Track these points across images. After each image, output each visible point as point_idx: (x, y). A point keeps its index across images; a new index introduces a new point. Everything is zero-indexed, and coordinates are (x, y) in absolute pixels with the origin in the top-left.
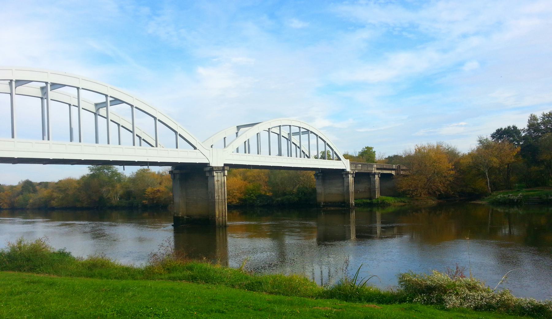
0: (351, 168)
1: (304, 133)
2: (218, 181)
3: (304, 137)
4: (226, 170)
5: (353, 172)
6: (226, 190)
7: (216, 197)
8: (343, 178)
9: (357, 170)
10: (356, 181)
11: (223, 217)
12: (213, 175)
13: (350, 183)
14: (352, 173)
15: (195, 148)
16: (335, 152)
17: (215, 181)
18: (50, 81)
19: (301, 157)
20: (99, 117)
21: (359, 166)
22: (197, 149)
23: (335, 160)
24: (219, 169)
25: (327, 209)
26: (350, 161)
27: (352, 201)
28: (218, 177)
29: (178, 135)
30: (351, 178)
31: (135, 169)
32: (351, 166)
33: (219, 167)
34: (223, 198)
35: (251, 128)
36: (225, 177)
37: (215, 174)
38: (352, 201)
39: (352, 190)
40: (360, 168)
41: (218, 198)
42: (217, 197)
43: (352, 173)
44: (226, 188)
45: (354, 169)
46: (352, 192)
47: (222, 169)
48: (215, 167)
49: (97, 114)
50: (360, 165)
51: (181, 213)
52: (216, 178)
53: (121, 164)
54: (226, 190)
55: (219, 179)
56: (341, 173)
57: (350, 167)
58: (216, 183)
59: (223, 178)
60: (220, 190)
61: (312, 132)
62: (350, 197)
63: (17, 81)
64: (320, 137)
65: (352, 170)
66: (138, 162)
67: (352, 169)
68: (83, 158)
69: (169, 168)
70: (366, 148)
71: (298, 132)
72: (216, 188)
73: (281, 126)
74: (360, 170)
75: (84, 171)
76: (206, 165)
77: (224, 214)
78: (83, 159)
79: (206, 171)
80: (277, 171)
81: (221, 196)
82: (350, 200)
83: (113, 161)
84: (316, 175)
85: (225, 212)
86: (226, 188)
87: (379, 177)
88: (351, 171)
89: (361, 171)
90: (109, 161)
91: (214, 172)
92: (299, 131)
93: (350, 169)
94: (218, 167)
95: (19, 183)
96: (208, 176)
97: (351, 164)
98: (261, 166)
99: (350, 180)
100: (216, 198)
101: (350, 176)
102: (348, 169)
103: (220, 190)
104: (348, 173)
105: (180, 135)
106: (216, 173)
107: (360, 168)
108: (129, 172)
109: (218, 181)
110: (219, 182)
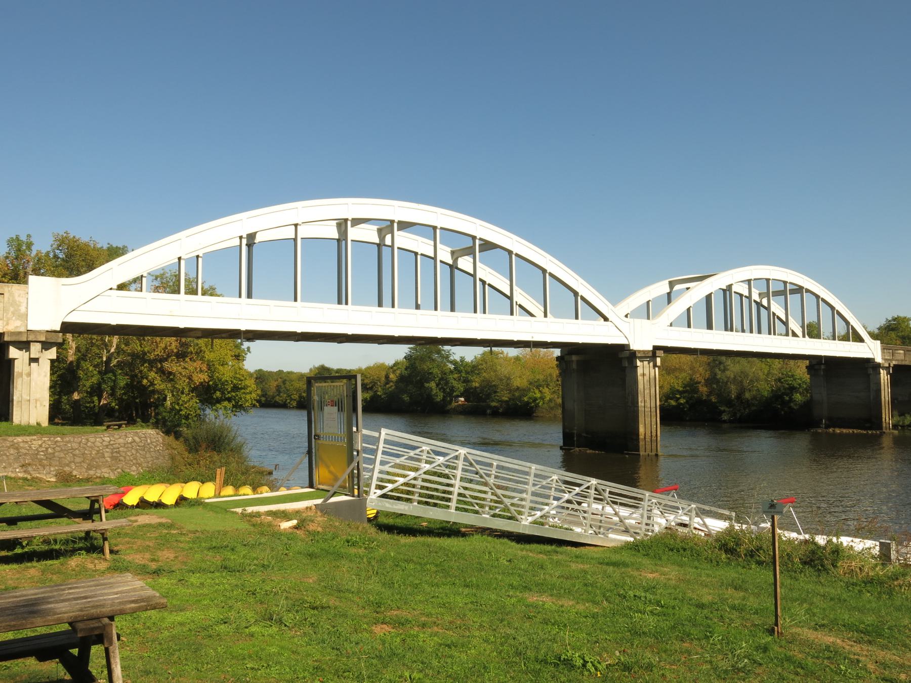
0: (885, 356)
1: (793, 292)
2: (644, 375)
3: (794, 300)
4: (659, 357)
5: (889, 364)
6: (658, 392)
7: (640, 404)
8: (868, 375)
9: (896, 360)
10: (894, 382)
11: (653, 438)
12: (634, 365)
13: (882, 384)
14: (887, 365)
15: (606, 319)
16: (852, 326)
17: (639, 374)
18: (805, 287)
19: (751, 332)
20: (456, 271)
21: (899, 353)
22: (610, 320)
23: (823, 339)
24: (647, 355)
25: (834, 431)
26: (881, 344)
27: (887, 419)
28: (644, 369)
29: (579, 298)
30: (884, 376)
31: (478, 351)
32: (883, 352)
33: (646, 351)
34: (653, 405)
35: (698, 285)
36: (657, 369)
37: (639, 363)
38: (887, 419)
39: (887, 399)
40: (902, 357)
41: (643, 404)
42: (641, 402)
43: (887, 365)
44: (657, 388)
45: (889, 358)
46: (887, 402)
47: (650, 354)
48: (639, 351)
49: (454, 266)
50: (902, 352)
51: (576, 428)
52: (640, 371)
53: (488, 345)
54: (658, 392)
55: (646, 372)
56: (865, 366)
57: (882, 355)
58: (640, 378)
59: (652, 371)
60: (647, 391)
61: (808, 291)
62: (883, 411)
63: (400, 223)
64: (823, 300)
65: (885, 360)
66: (302, 333)
67: (886, 357)
68: (397, 333)
69: (557, 352)
70: (894, 319)
71: (471, 247)
72: (641, 386)
73: (751, 280)
74: (902, 360)
75: (399, 353)
76: (623, 348)
77: (654, 434)
78: (300, 332)
79: (622, 358)
80: (729, 362)
81: (648, 401)
82: (884, 416)
83: (185, 328)
84: (810, 368)
85: (657, 430)
86: (657, 388)
87: (890, 374)
88: (883, 362)
89: (904, 363)
90: (753, 352)
91: (638, 360)
92: (472, 245)
93: (882, 359)
94: (644, 352)
95: (311, 370)
96: (626, 367)
97: (883, 349)
98: (809, 355)
99: (882, 378)
100: (641, 404)
101: (883, 373)
102: (879, 359)
103: (647, 391)
104: (878, 366)
105: (583, 299)
106: (640, 361)
107: (902, 357)
108: (470, 354)
109: (644, 375)
110: (646, 378)
